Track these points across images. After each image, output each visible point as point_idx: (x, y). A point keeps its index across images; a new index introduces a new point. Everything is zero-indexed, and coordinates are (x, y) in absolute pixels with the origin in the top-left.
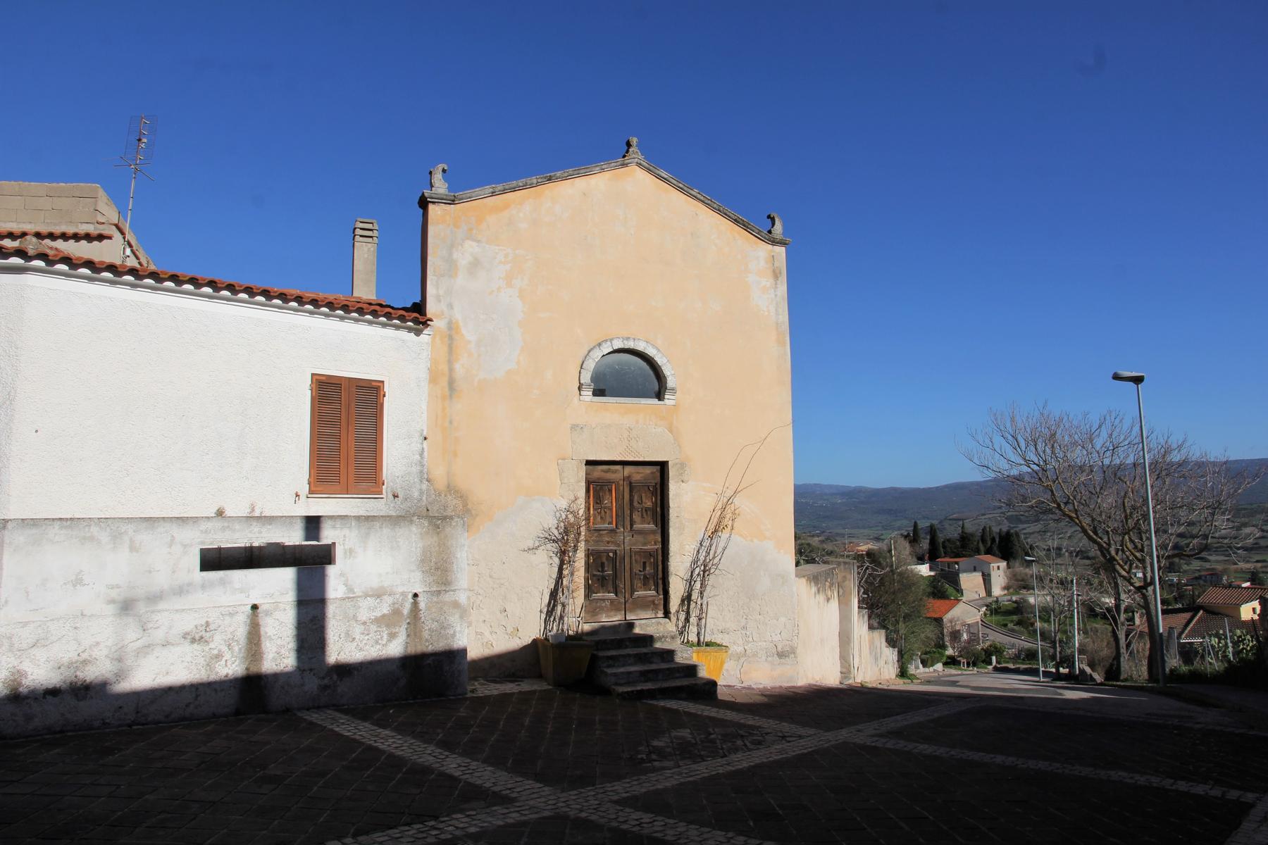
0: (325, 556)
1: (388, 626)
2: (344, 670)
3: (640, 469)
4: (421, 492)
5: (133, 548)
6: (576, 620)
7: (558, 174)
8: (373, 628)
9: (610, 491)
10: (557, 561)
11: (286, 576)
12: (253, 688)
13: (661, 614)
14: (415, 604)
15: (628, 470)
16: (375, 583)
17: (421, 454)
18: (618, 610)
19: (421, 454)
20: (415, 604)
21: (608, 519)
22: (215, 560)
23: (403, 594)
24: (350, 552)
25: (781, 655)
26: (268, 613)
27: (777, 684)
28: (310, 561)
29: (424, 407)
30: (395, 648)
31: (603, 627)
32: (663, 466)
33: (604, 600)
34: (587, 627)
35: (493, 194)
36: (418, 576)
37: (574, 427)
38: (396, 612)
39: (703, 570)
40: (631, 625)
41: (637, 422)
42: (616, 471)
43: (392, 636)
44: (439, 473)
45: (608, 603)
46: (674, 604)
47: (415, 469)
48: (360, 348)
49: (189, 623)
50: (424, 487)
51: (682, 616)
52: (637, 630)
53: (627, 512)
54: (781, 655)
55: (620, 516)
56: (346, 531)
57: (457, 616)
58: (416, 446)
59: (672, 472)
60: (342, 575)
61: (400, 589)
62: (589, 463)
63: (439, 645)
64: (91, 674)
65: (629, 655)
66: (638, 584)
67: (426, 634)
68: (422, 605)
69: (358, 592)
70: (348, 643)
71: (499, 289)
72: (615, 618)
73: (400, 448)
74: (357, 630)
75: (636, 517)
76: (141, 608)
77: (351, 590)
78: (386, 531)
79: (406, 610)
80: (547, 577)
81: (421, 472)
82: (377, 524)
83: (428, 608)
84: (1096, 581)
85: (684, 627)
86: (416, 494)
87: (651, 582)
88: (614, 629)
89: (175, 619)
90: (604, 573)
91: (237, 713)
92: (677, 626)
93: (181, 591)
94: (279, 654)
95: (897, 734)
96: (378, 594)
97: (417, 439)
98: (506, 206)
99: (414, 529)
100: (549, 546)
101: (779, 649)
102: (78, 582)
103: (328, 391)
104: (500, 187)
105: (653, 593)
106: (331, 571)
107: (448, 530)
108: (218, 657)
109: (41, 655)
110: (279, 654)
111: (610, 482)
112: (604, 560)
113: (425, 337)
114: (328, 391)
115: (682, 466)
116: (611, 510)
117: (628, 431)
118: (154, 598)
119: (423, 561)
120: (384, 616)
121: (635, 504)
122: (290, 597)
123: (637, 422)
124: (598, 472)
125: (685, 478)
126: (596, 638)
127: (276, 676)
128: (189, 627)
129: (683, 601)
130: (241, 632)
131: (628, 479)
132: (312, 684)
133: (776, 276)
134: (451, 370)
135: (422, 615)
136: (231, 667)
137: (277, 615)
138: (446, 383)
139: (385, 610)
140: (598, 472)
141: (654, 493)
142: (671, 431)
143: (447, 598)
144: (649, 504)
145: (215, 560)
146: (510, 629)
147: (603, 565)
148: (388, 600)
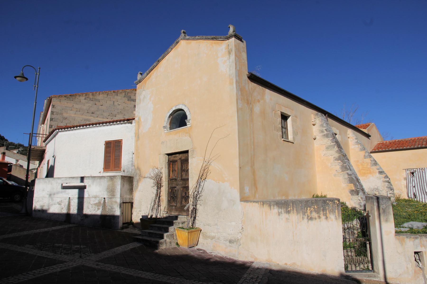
0: (85, 187)
1: (98, 206)
2: (87, 216)
4: (132, 170)
5: (51, 184)
7: (160, 58)
8: (94, 206)
11: (77, 191)
12: (68, 216)
14: (105, 201)
16: (95, 194)
17: (132, 158)
19: (132, 158)
20: (105, 201)
22: (64, 188)
23: (102, 198)
24: (90, 186)
25: (230, 242)
26: (72, 200)
27: (228, 257)
28: (82, 189)
29: (134, 144)
30: (99, 212)
35: (148, 74)
36: (106, 193)
38: (100, 203)
43: (98, 209)
44: (136, 164)
45: (174, 207)
47: (130, 163)
48: (113, 132)
49: (59, 200)
50: (133, 168)
54: (230, 242)
56: (89, 180)
57: (116, 206)
58: (131, 156)
60: (88, 191)
61: (101, 196)
62: (169, 155)
63: (111, 213)
64: (45, 208)
65: (156, 226)
67: (107, 210)
68: (106, 201)
69: (91, 196)
70: (88, 210)
73: (126, 158)
74: (90, 206)
76: (52, 196)
77: (89, 195)
78: (98, 180)
79: (102, 202)
81: (132, 164)
82: (96, 178)
83: (108, 202)
84: (312, 209)
86: (131, 170)
89: (57, 198)
91: (65, 222)
93: (58, 193)
94: (74, 210)
95: (53, 262)
96: (95, 197)
97: (131, 154)
98: (151, 76)
99: (105, 179)
102: (43, 190)
103: (108, 144)
104: (148, 71)
106: (86, 190)
107: (115, 180)
108: (63, 208)
109: (38, 203)
110: (74, 210)
111: (176, 161)
113: (134, 124)
114: (108, 144)
117: (178, 140)
118: (54, 194)
119: (107, 189)
120: (97, 203)
122: (77, 196)
126: (167, 220)
127: (73, 215)
128: (58, 201)
130: (67, 203)
132: (79, 218)
133: (229, 53)
134: (138, 132)
135: (106, 204)
136: (65, 211)
137: (74, 200)
138: (137, 136)
139: (97, 202)
140: (172, 158)
143: (114, 200)
145: (64, 188)
148: (98, 199)
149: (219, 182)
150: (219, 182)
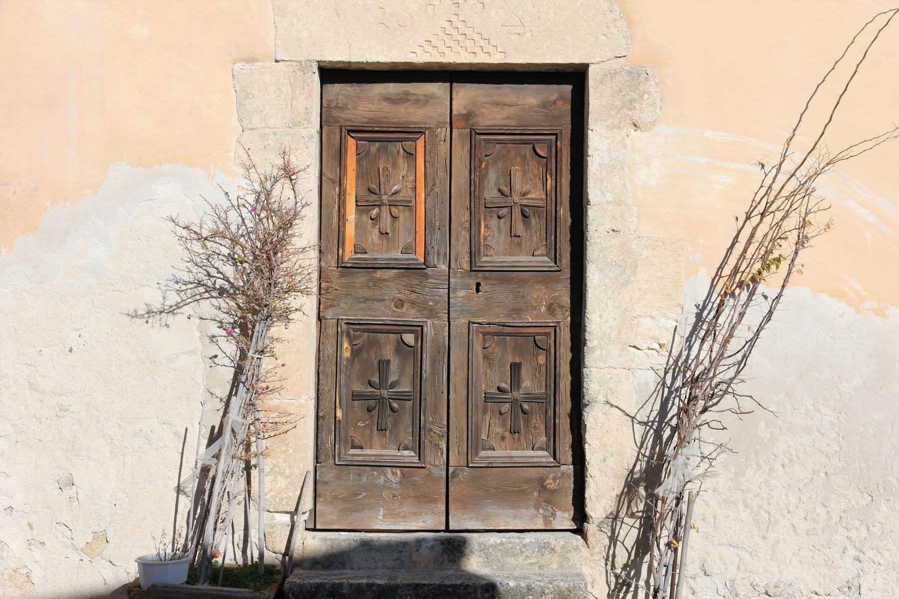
3: (507, 92)
6: (275, 513)
9: (411, 155)
10: (230, 348)
13: (564, 519)
15: (466, 95)
18: (423, 499)
21: (404, 238)
31: (366, 545)
32: (575, 77)
33: (378, 466)
34: (310, 543)
39: (687, 396)
40: (453, 547)
42: (427, 99)
46: (601, 496)
51: (629, 533)
52: (476, 564)
53: (461, 216)
55: (440, 226)
62: (330, 74)
66: (491, 426)
72: (421, 522)
75: (494, 233)
80: (200, 393)
85: (633, 565)
87: (537, 421)
88: (400, 553)
90: (375, 389)
92: (611, 559)
100: (207, 307)
105: (544, 456)
112: (388, 353)
115: (636, 77)
116: (409, 206)
121: (490, 194)
125: (644, 116)
129: (630, 486)
141: (550, 164)
144: (536, 195)
146: (83, 538)
147: (383, 365)
149: (880, 312)
150: (880, 312)
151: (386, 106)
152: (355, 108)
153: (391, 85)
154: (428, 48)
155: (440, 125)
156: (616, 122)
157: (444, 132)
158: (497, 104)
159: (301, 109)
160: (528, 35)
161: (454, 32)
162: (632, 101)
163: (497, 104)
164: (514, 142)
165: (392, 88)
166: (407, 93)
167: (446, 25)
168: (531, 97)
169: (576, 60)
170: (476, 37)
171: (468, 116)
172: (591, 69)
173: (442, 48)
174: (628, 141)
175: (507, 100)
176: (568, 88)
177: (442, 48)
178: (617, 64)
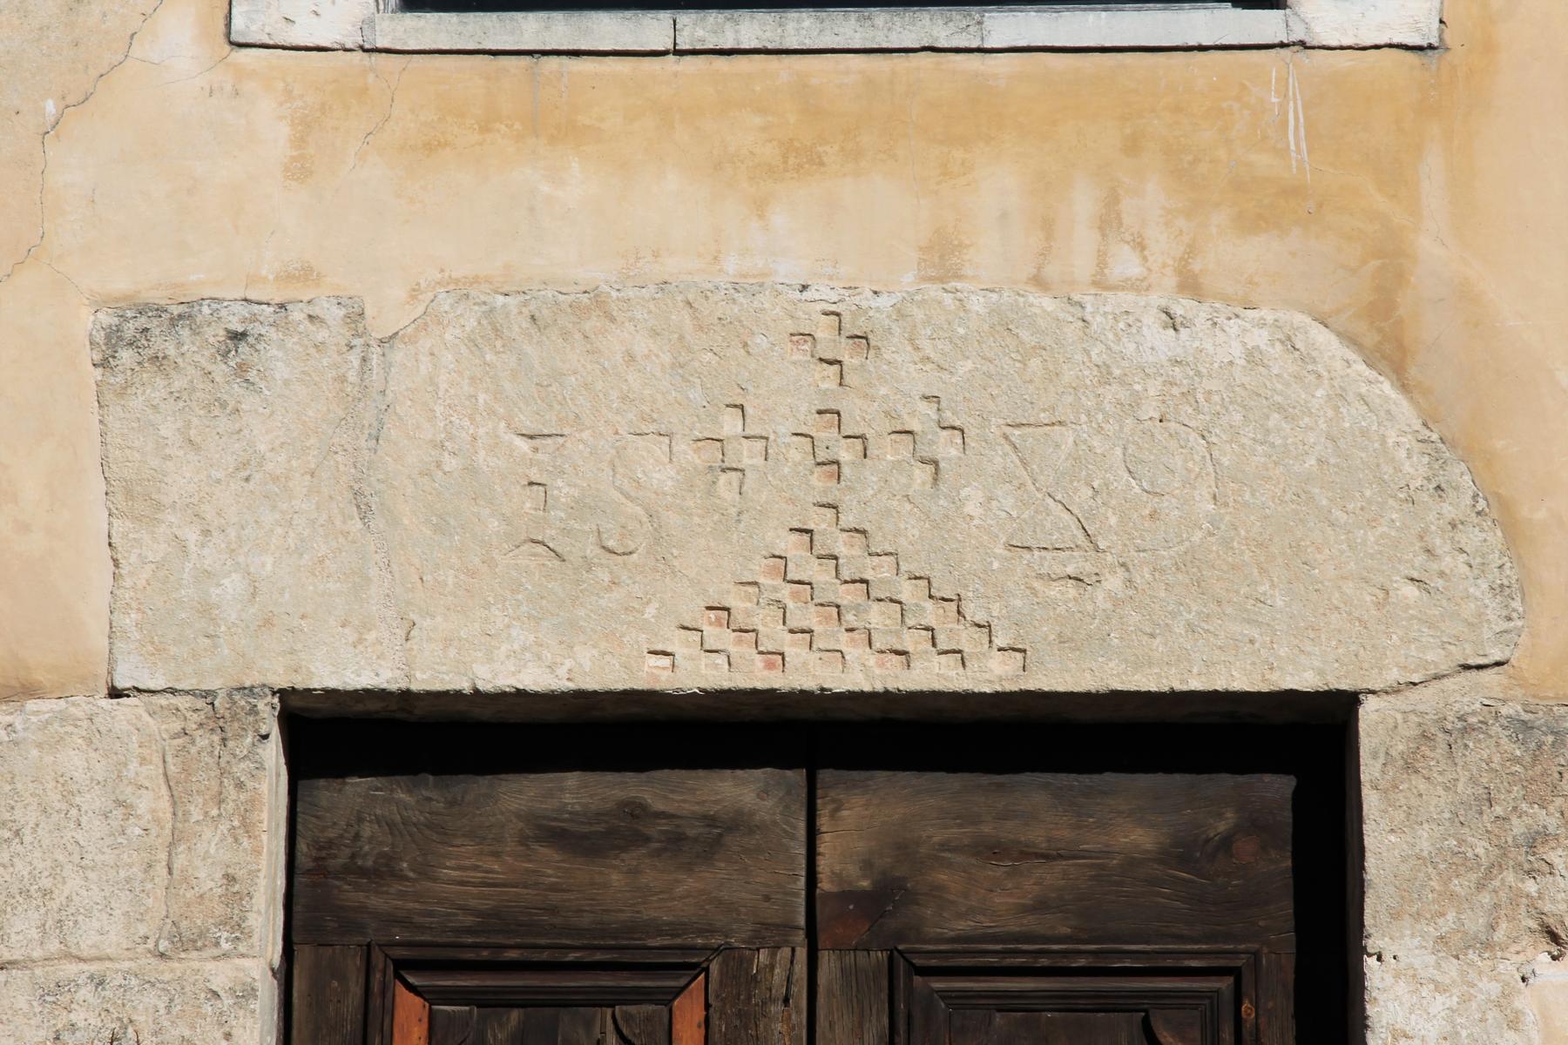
3: (1037, 807)
15: (864, 821)
32: (1305, 743)
37: (136, 335)
41: (943, 259)
42: (716, 837)
59: (1395, 836)
62: (332, 738)
71: (1492, 928)
101: (1196, 266)
123: (943, 259)
124: (485, 849)
131: (871, 921)
142: (1392, 354)
151: (551, 864)
152: (425, 871)
153: (572, 779)
154: (716, 635)
155: (770, 934)
156: (1475, 923)
157: (782, 967)
158: (992, 851)
159: (208, 880)
160: (1114, 582)
161: (821, 574)
162: (1536, 840)
163: (992, 851)
164: (1067, 1003)
165: (575, 792)
166: (635, 811)
167: (791, 545)
168: (1128, 822)
169: (1305, 679)
170: (841, 545)
171: (883, 901)
172: (1370, 713)
173: (774, 634)
174: (1524, 1001)
175: (1036, 836)
176: (1277, 788)
177: (774, 634)
178: (1466, 695)
